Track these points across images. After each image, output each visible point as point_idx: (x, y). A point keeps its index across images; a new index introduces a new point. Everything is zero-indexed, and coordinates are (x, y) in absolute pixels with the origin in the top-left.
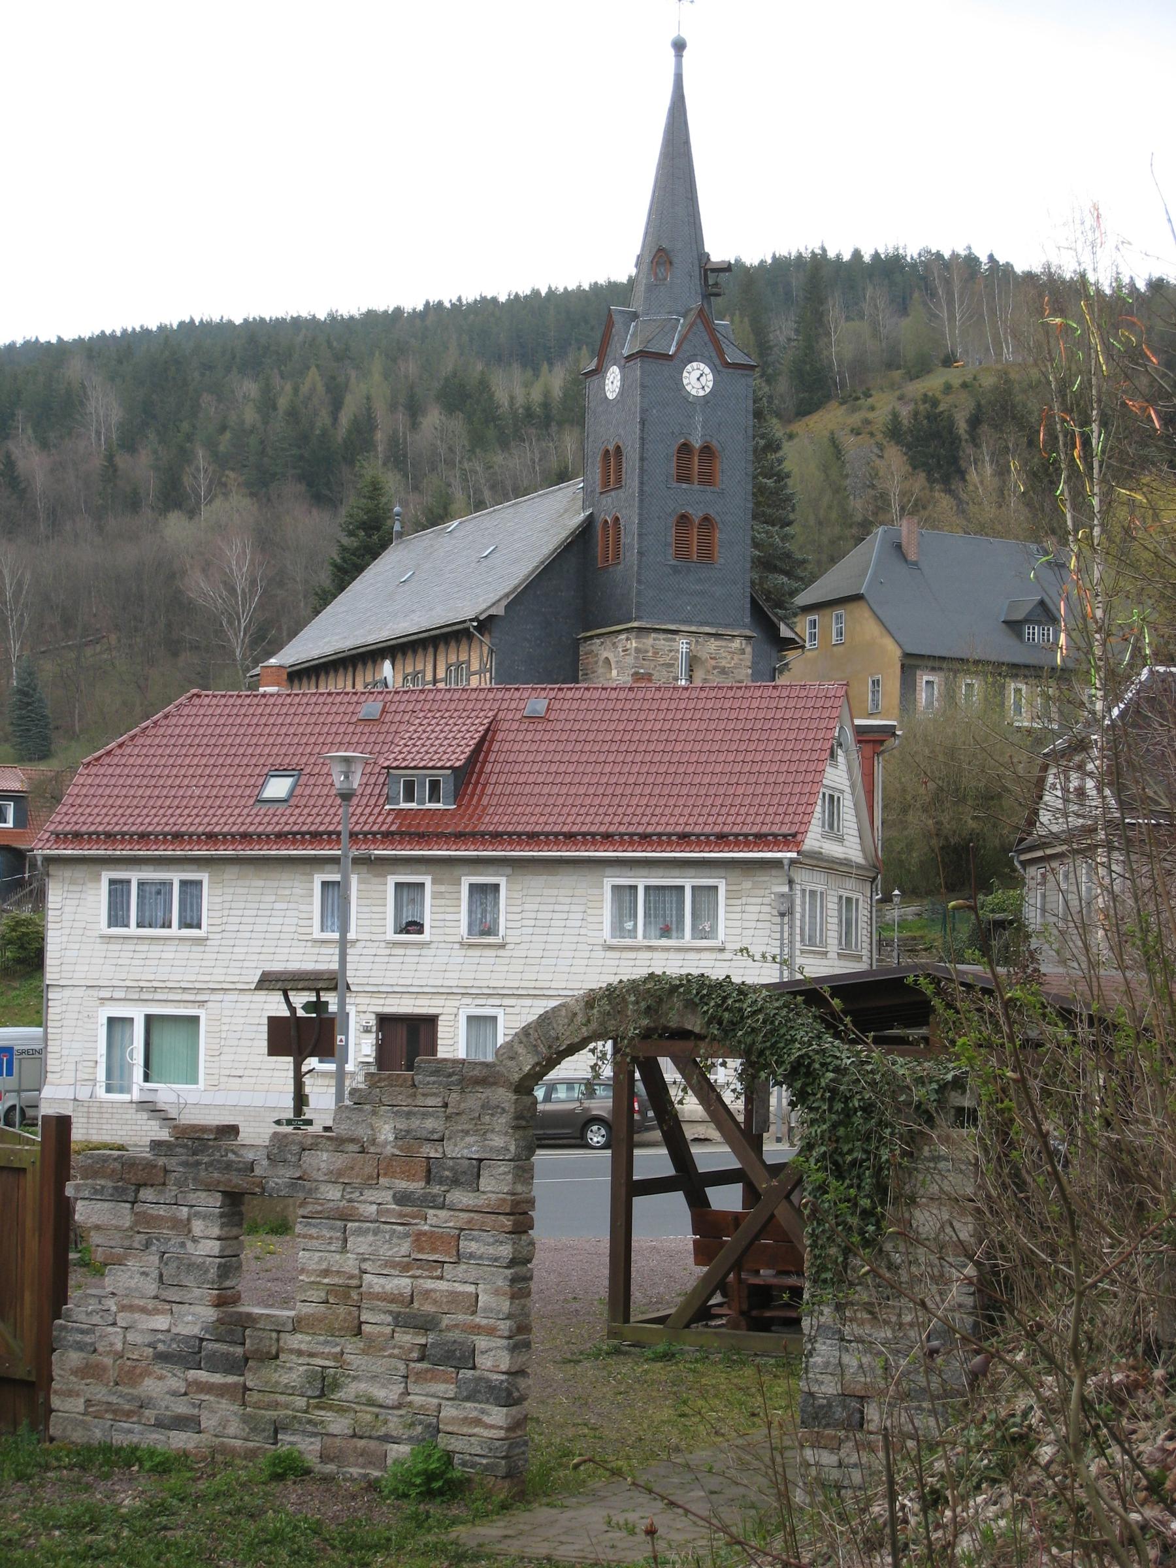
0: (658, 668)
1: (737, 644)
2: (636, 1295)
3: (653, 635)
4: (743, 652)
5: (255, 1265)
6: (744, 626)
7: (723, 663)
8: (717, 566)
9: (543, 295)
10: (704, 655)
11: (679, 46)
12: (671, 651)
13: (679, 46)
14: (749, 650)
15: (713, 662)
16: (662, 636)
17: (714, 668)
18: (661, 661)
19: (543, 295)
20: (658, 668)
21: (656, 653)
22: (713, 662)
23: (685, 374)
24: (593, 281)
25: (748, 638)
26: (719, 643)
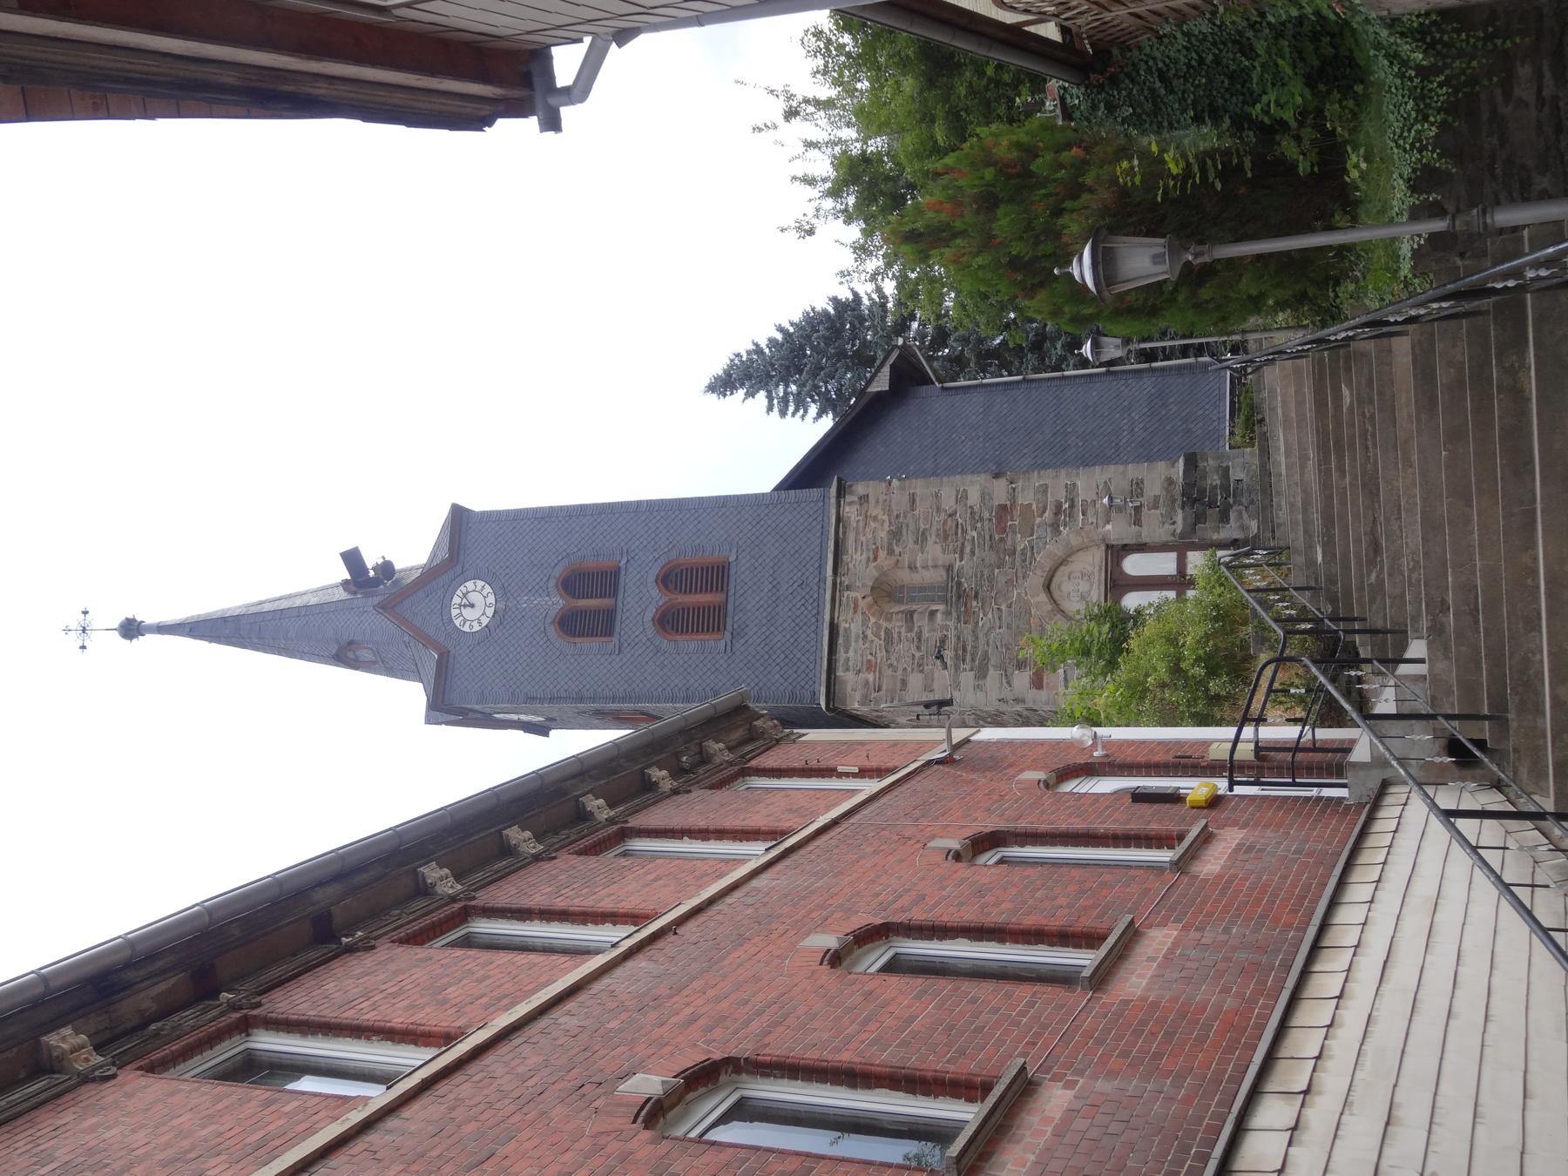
0: (893, 660)
1: (851, 512)
2: (1236, 753)
3: (840, 673)
4: (864, 499)
5: (1028, 1139)
6: (824, 497)
7: (883, 535)
8: (732, 559)
9: (349, 577)
10: (872, 572)
11: (131, 629)
12: (865, 637)
13: (131, 629)
14: (860, 488)
15: (882, 554)
16: (841, 656)
17: (891, 552)
18: (881, 654)
19: (349, 577)
20: (893, 660)
21: (870, 667)
22: (882, 554)
23: (466, 629)
24: (131, 617)
25: (841, 493)
26: (851, 549)
